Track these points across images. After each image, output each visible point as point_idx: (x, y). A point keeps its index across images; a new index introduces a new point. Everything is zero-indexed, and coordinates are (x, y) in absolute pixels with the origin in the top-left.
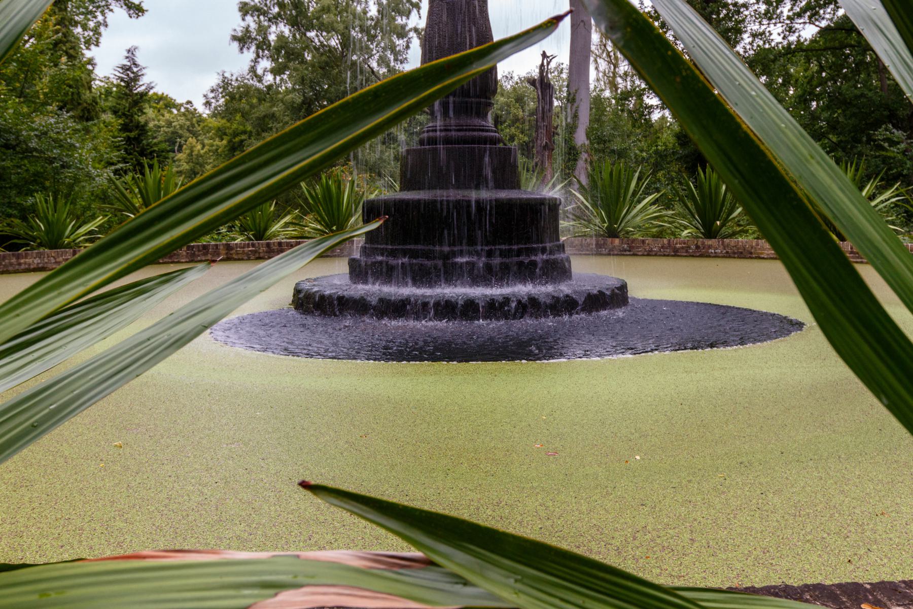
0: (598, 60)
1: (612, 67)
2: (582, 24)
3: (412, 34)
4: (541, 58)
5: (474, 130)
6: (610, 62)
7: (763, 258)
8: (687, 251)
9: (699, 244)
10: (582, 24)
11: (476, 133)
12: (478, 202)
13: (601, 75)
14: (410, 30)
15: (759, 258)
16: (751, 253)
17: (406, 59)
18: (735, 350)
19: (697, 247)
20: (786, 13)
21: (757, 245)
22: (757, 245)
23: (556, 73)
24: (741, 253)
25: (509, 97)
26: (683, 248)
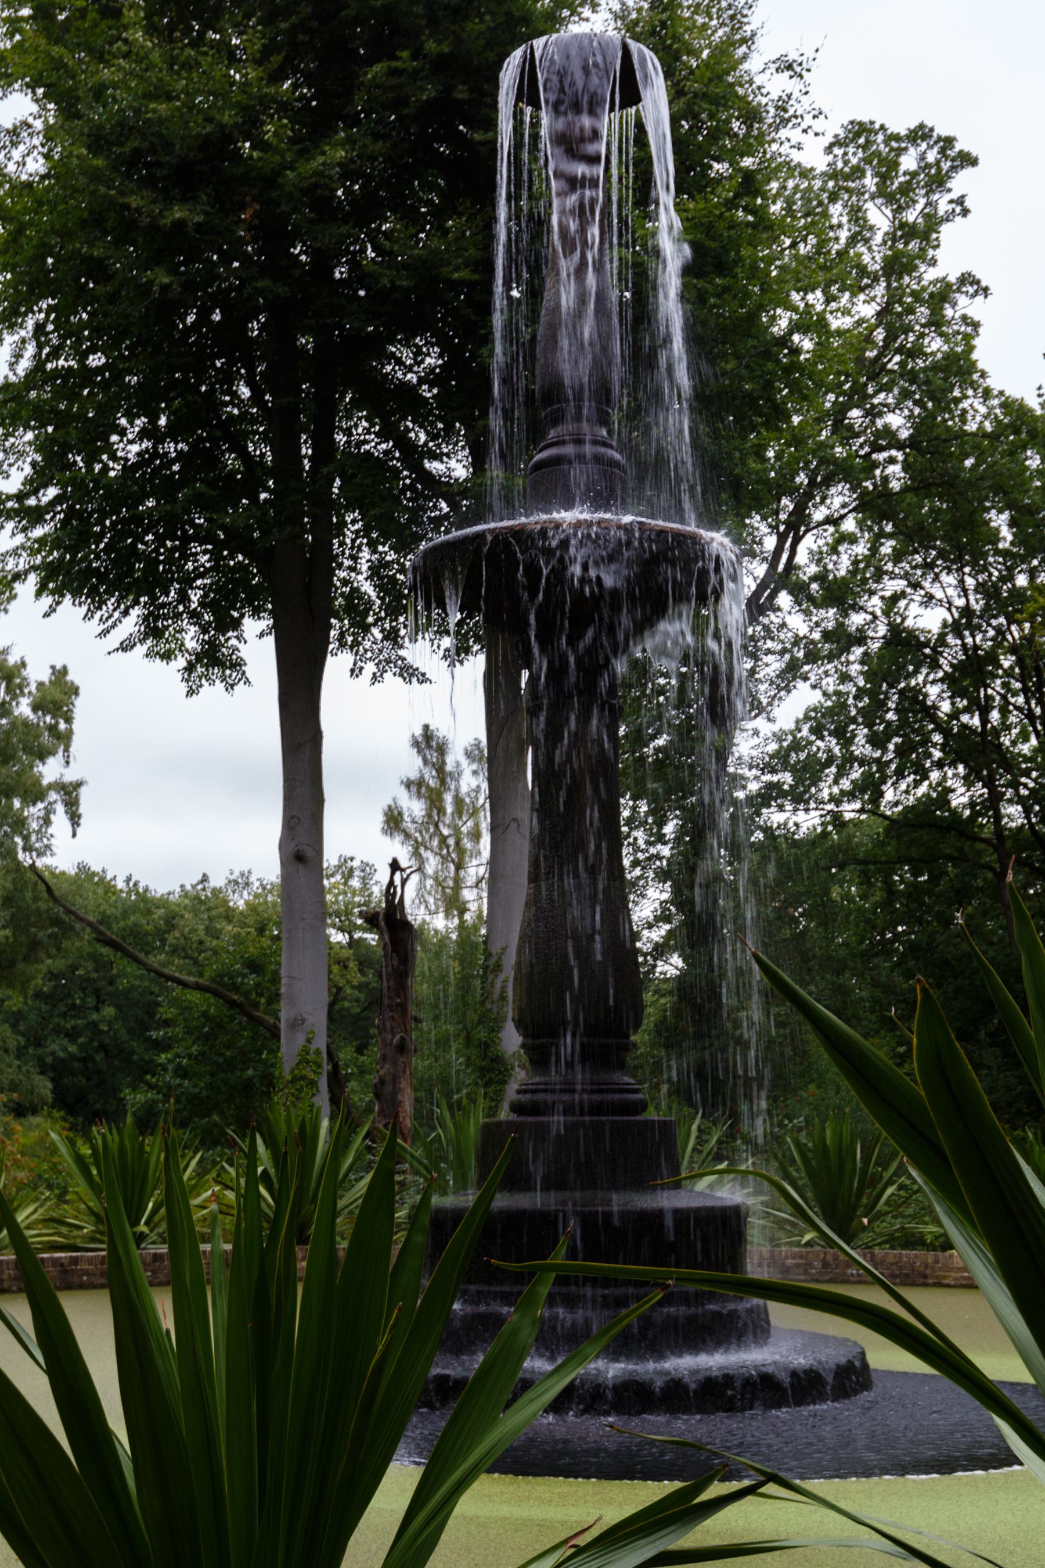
0: (422, 850)
1: (452, 867)
2: (514, 825)
3: (53, 796)
4: (388, 871)
5: (614, 1091)
6: (445, 859)
7: (948, 1286)
8: (806, 1273)
9: (829, 1258)
10: (514, 825)
11: (617, 1096)
12: (677, 1212)
13: (429, 882)
14: (50, 786)
15: (940, 1285)
16: (925, 1276)
17: (48, 847)
18: (569, 1485)
19: (825, 1265)
20: (825, 794)
21: (937, 1261)
22: (937, 1261)
23: (338, 877)
24: (907, 1276)
25: (244, 925)
26: (798, 1266)
